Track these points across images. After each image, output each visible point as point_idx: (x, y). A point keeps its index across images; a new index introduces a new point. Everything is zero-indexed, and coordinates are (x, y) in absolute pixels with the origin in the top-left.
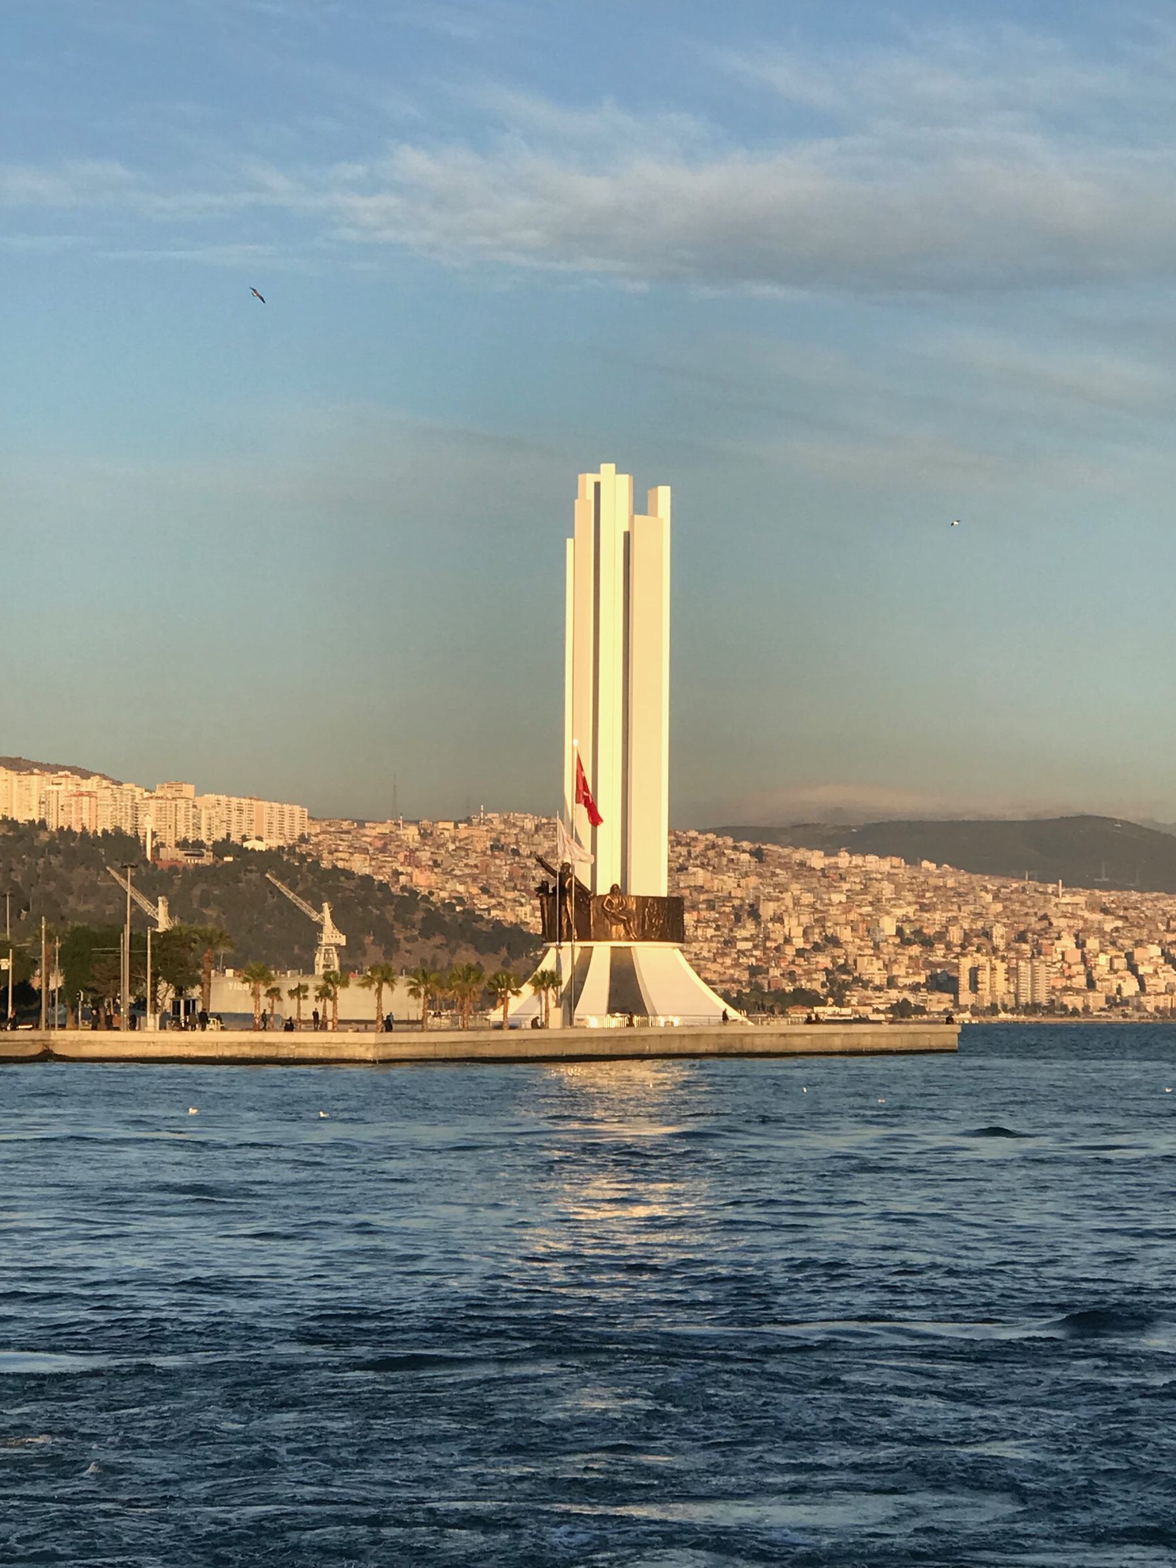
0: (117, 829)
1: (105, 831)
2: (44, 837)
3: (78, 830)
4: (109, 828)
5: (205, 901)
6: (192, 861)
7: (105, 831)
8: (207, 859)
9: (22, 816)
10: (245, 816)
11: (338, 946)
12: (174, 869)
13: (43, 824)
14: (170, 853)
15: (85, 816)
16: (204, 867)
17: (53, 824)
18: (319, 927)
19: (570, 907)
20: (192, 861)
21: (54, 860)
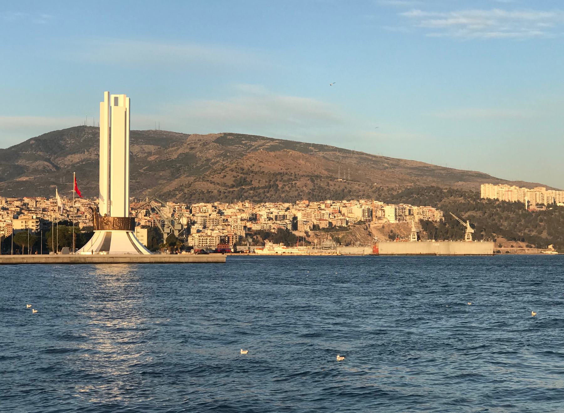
0: (518, 201)
1: (515, 202)
2: (497, 203)
3: (507, 201)
4: (516, 200)
5: (541, 221)
6: (539, 209)
7: (515, 202)
8: (544, 209)
9: (492, 197)
10: (561, 196)
11: (471, 233)
12: (533, 212)
13: (498, 200)
14: (533, 207)
15: (510, 197)
16: (543, 211)
17: (500, 199)
18: (466, 228)
19: (100, 222)
20: (539, 209)
21: (498, 209)
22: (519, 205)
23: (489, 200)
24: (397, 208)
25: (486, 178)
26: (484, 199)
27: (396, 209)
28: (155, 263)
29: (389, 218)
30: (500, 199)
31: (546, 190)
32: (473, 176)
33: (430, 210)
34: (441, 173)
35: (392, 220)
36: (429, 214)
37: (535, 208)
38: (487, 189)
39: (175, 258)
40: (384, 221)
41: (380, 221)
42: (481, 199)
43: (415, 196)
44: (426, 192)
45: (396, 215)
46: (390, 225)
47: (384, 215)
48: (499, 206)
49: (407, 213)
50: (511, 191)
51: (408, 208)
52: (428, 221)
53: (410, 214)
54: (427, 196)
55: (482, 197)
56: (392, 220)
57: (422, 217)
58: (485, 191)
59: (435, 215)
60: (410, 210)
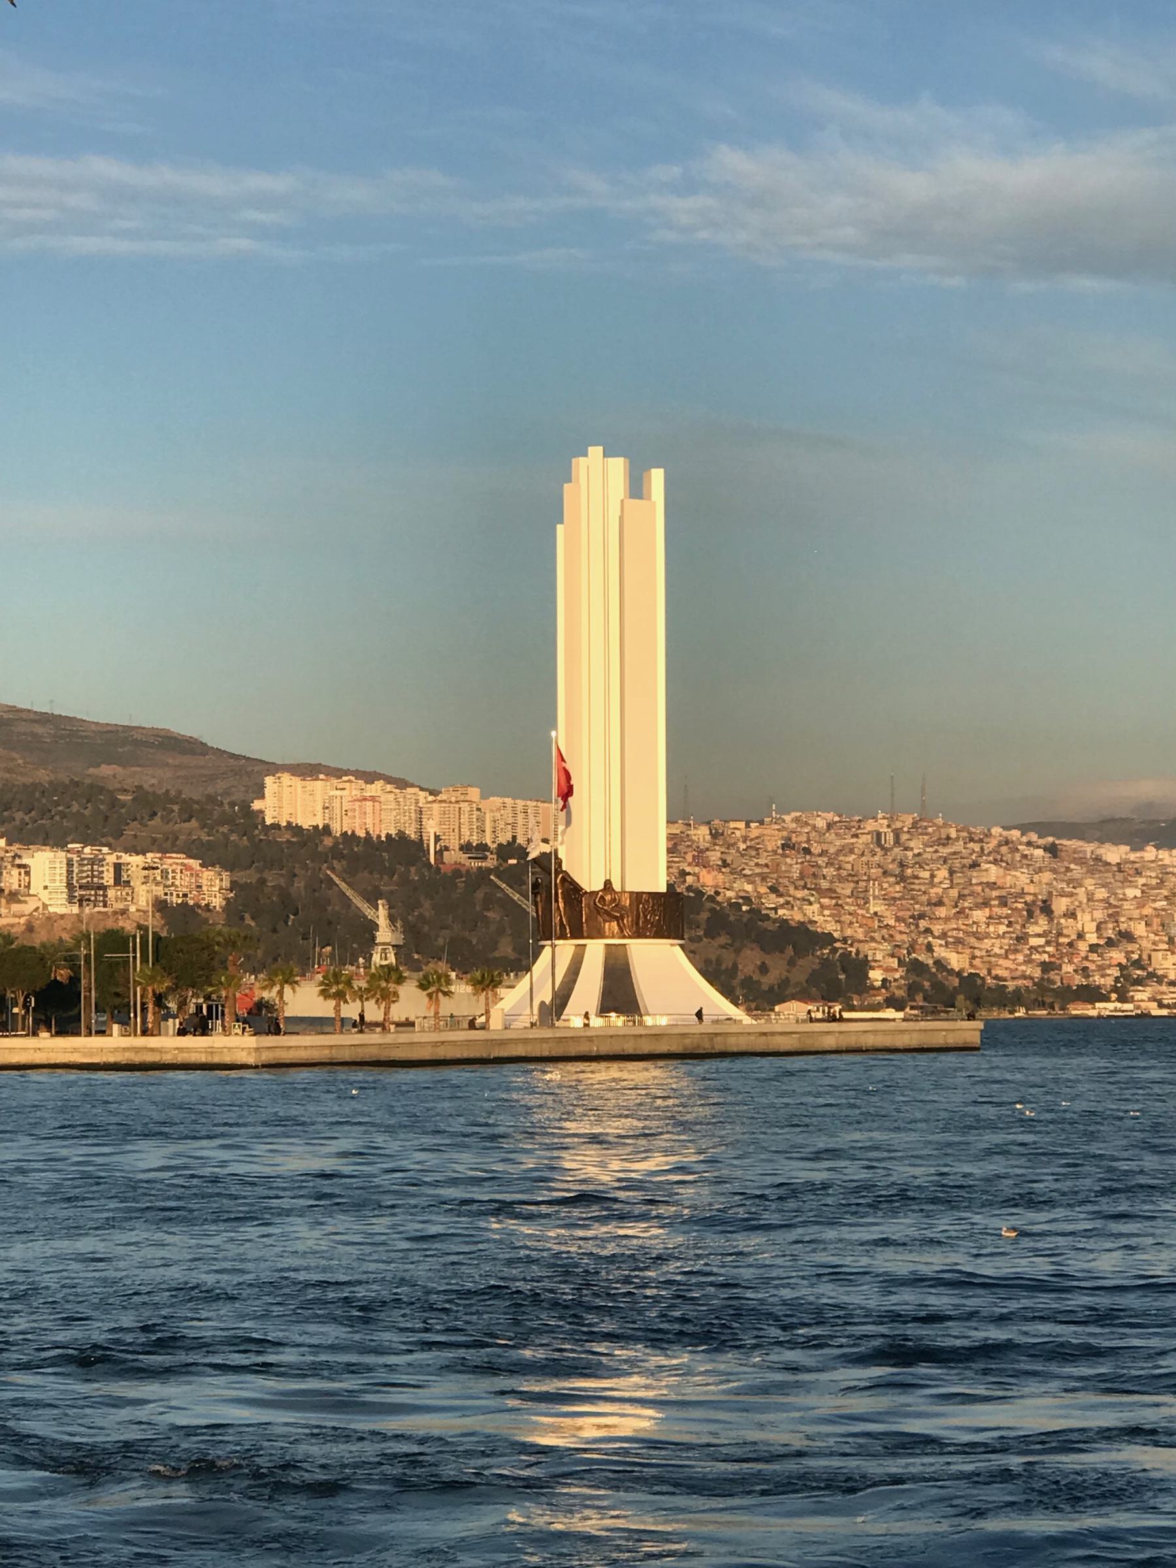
0: (401, 834)
1: (388, 836)
2: (328, 842)
3: (362, 834)
4: (393, 832)
6: (475, 864)
7: (388, 836)
8: (491, 862)
9: (306, 822)
12: (457, 873)
13: (327, 830)
14: (454, 857)
15: (369, 821)
17: (337, 830)
20: (475, 864)
22: (405, 848)
23: (296, 830)
24: (75, 858)
25: (193, 752)
26: (276, 826)
27: (70, 864)
28: (849, 1051)
29: (44, 896)
30: (337, 830)
31: (263, 797)
32: (147, 744)
33: (188, 868)
34: (34, 735)
35: (59, 905)
36: (183, 882)
37: (463, 858)
38: (286, 790)
39: (196, 1047)
40: (28, 908)
41: (15, 907)
42: (267, 829)
43: (19, 815)
44: (57, 804)
45: (70, 886)
46: (51, 919)
47: (28, 887)
48: (335, 852)
49: (108, 878)
50: (373, 799)
51: (111, 859)
52: (184, 905)
53: (118, 880)
54: (63, 816)
55: (268, 821)
56: (59, 905)
57: (159, 891)
58: (280, 800)
59: (204, 882)
60: (118, 868)
